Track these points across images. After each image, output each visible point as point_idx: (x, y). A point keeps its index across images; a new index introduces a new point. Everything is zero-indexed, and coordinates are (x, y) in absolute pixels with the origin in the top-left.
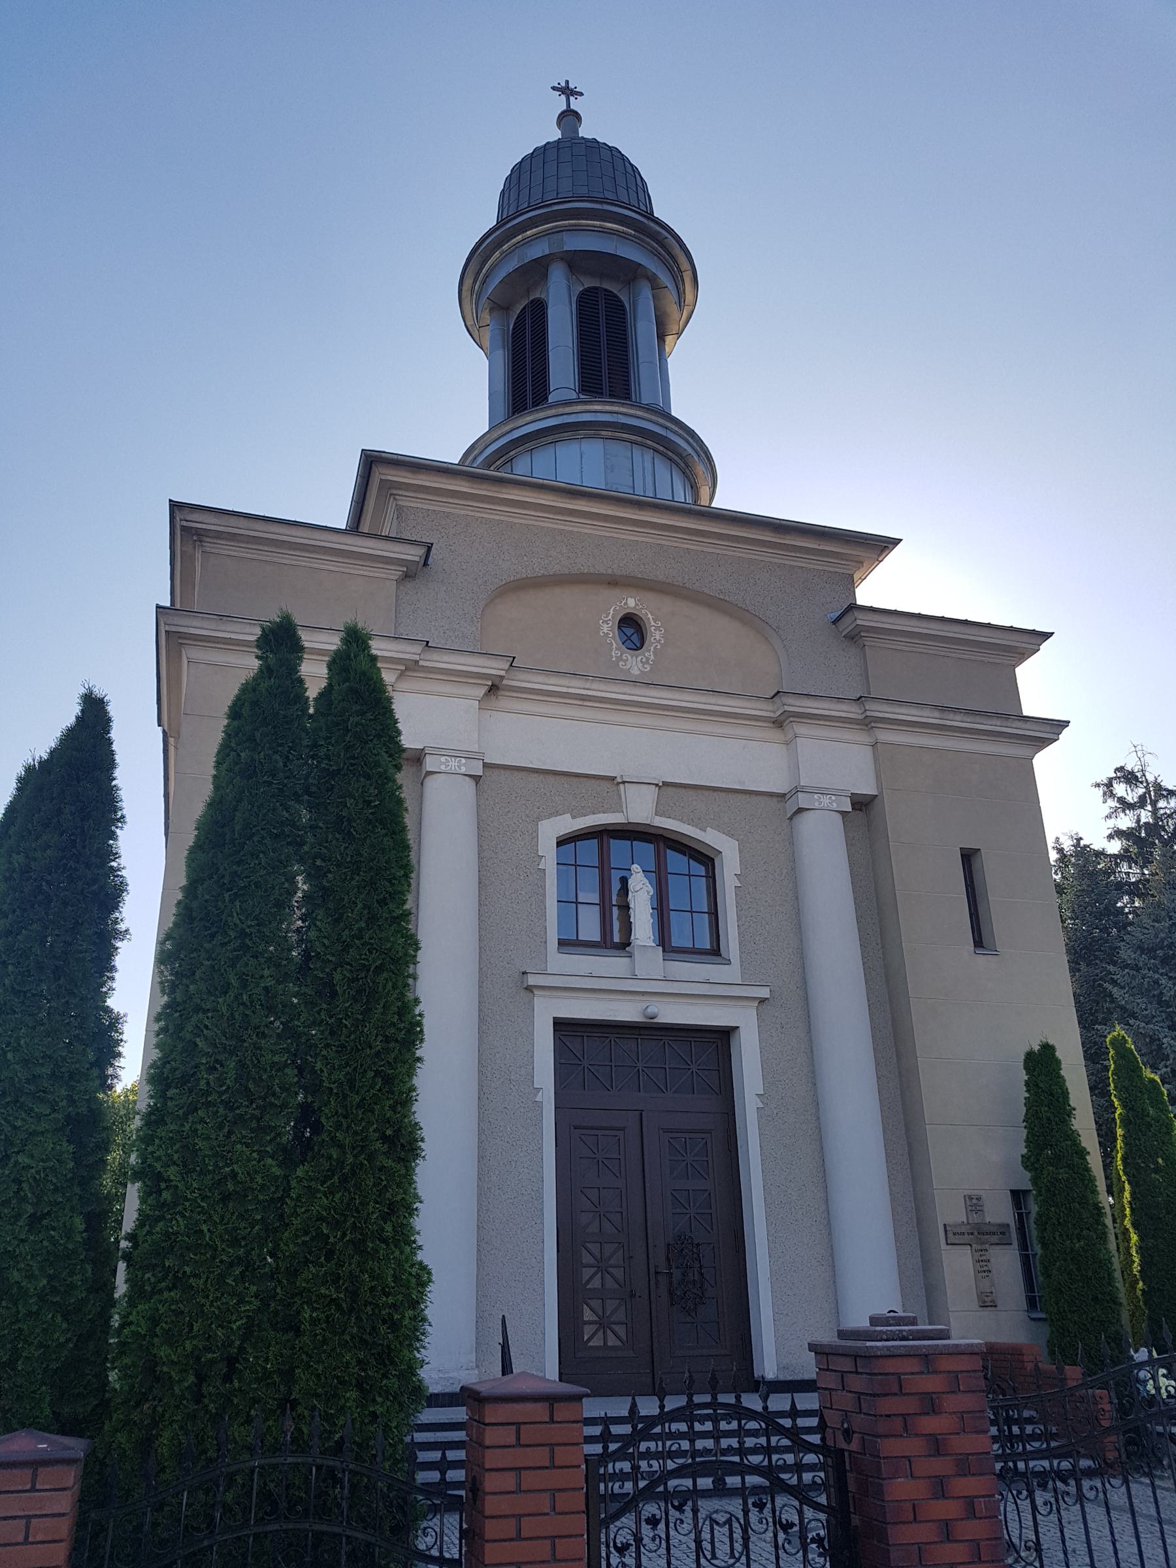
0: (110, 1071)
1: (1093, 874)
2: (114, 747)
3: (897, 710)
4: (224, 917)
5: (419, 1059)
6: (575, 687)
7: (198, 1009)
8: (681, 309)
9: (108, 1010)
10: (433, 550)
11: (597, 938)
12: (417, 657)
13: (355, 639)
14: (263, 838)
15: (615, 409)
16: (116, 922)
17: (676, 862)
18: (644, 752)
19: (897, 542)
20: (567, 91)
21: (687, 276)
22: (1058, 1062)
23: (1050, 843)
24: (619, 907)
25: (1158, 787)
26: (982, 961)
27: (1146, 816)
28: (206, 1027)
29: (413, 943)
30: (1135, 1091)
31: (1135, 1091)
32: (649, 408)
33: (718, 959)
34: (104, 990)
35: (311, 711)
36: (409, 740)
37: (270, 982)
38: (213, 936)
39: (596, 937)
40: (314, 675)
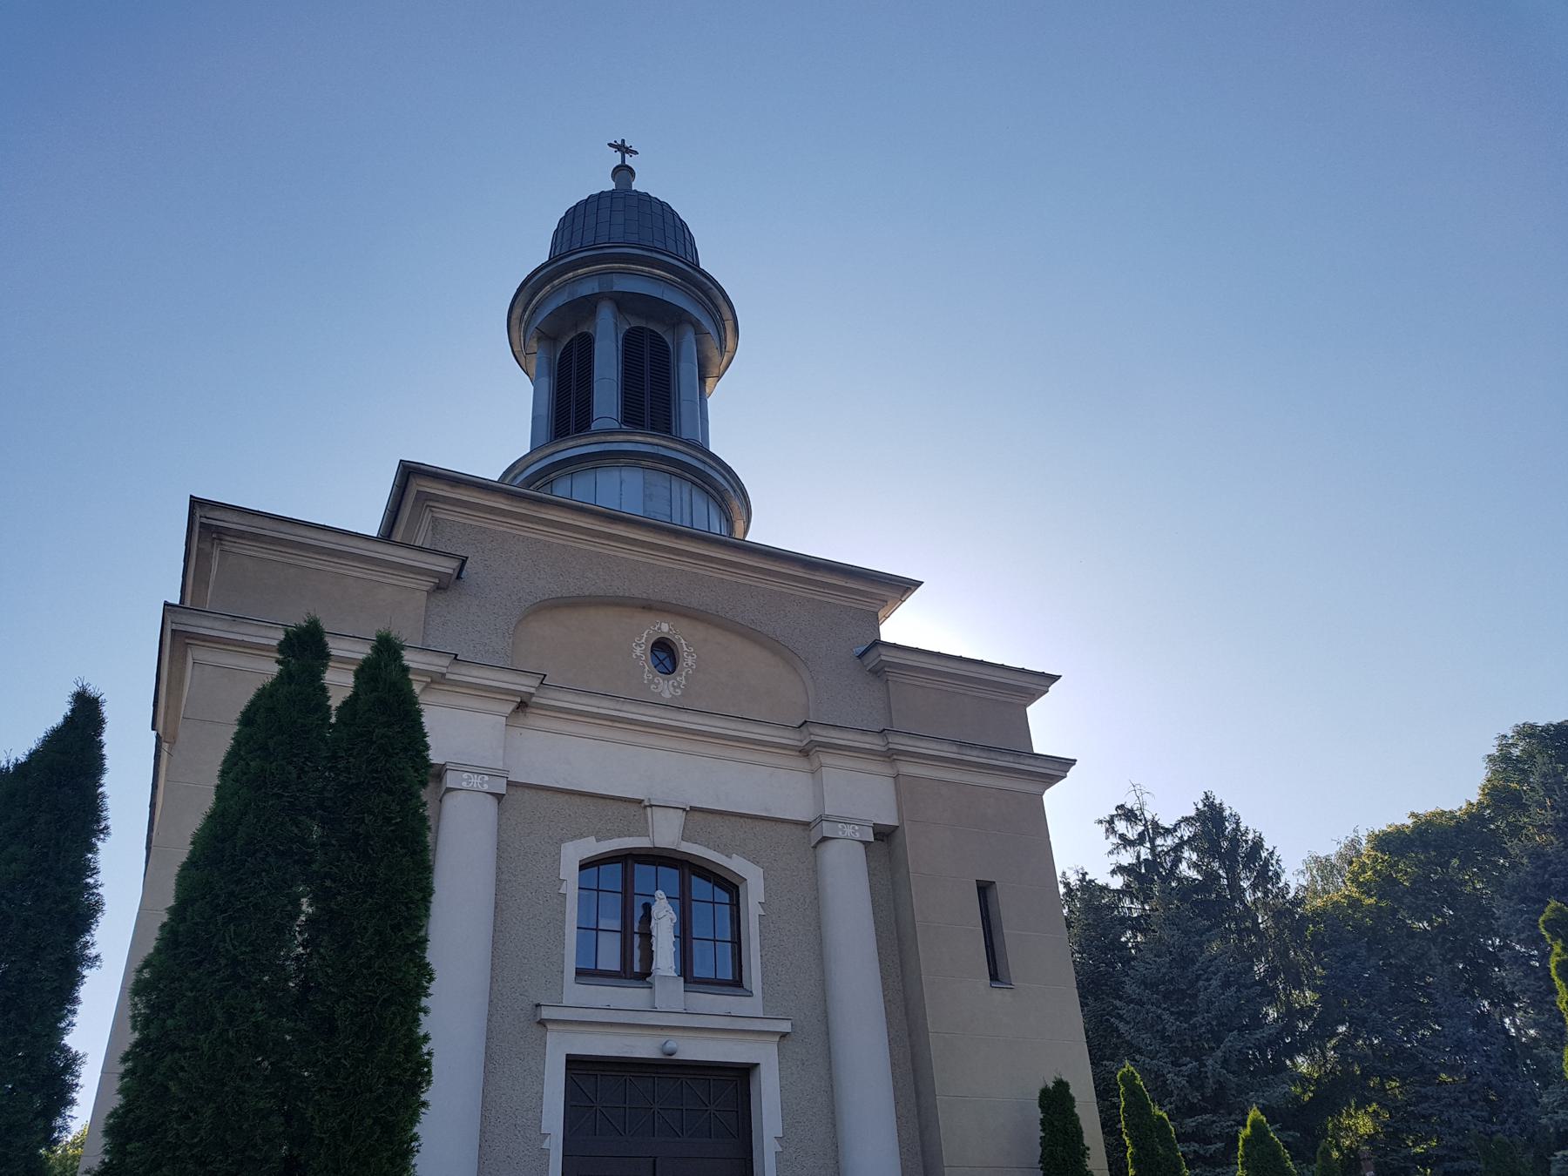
0: (59, 1122)
1: (1098, 909)
2: (105, 751)
4: (214, 943)
5: (424, 1104)
6: (606, 707)
7: (174, 1048)
8: (722, 355)
9: (65, 1050)
10: (468, 564)
11: (616, 967)
13: (387, 649)
14: (267, 855)
15: (656, 441)
16: (86, 946)
17: (700, 888)
18: (671, 778)
19: (918, 584)
20: (623, 149)
21: (729, 325)
22: (1072, 1099)
23: (1059, 874)
24: (641, 935)
25: (1155, 824)
26: (999, 995)
27: (1145, 853)
28: (182, 1069)
29: (425, 972)
30: (1145, 1130)
31: (1145, 1130)
32: (689, 443)
33: (739, 991)
34: (63, 1025)
35: (333, 720)
36: (435, 757)
37: (261, 1017)
38: (200, 963)
39: (616, 967)
40: (339, 683)
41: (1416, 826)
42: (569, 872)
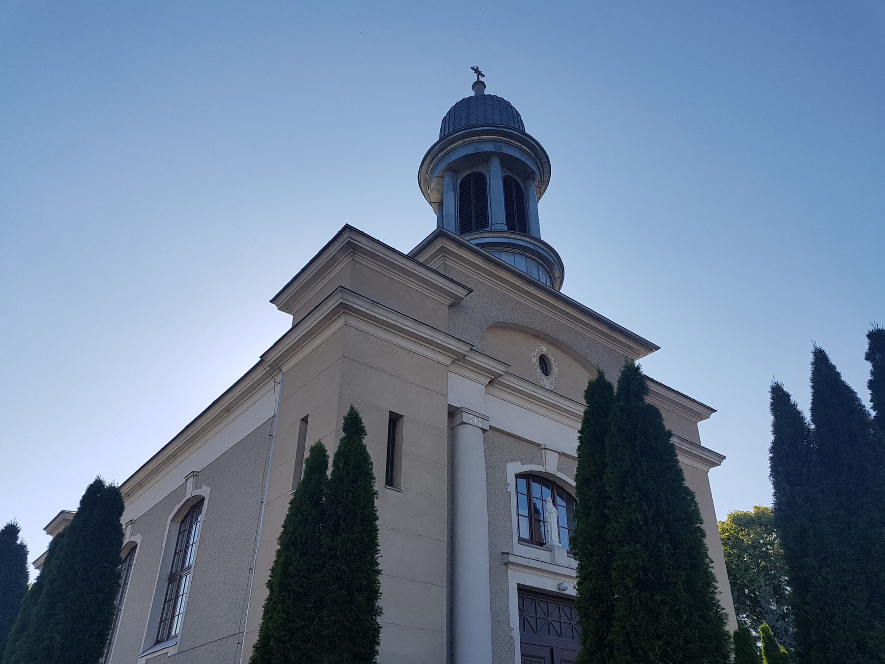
12: (466, 353)
19: (657, 348)
41: (756, 514)
42: (511, 479)
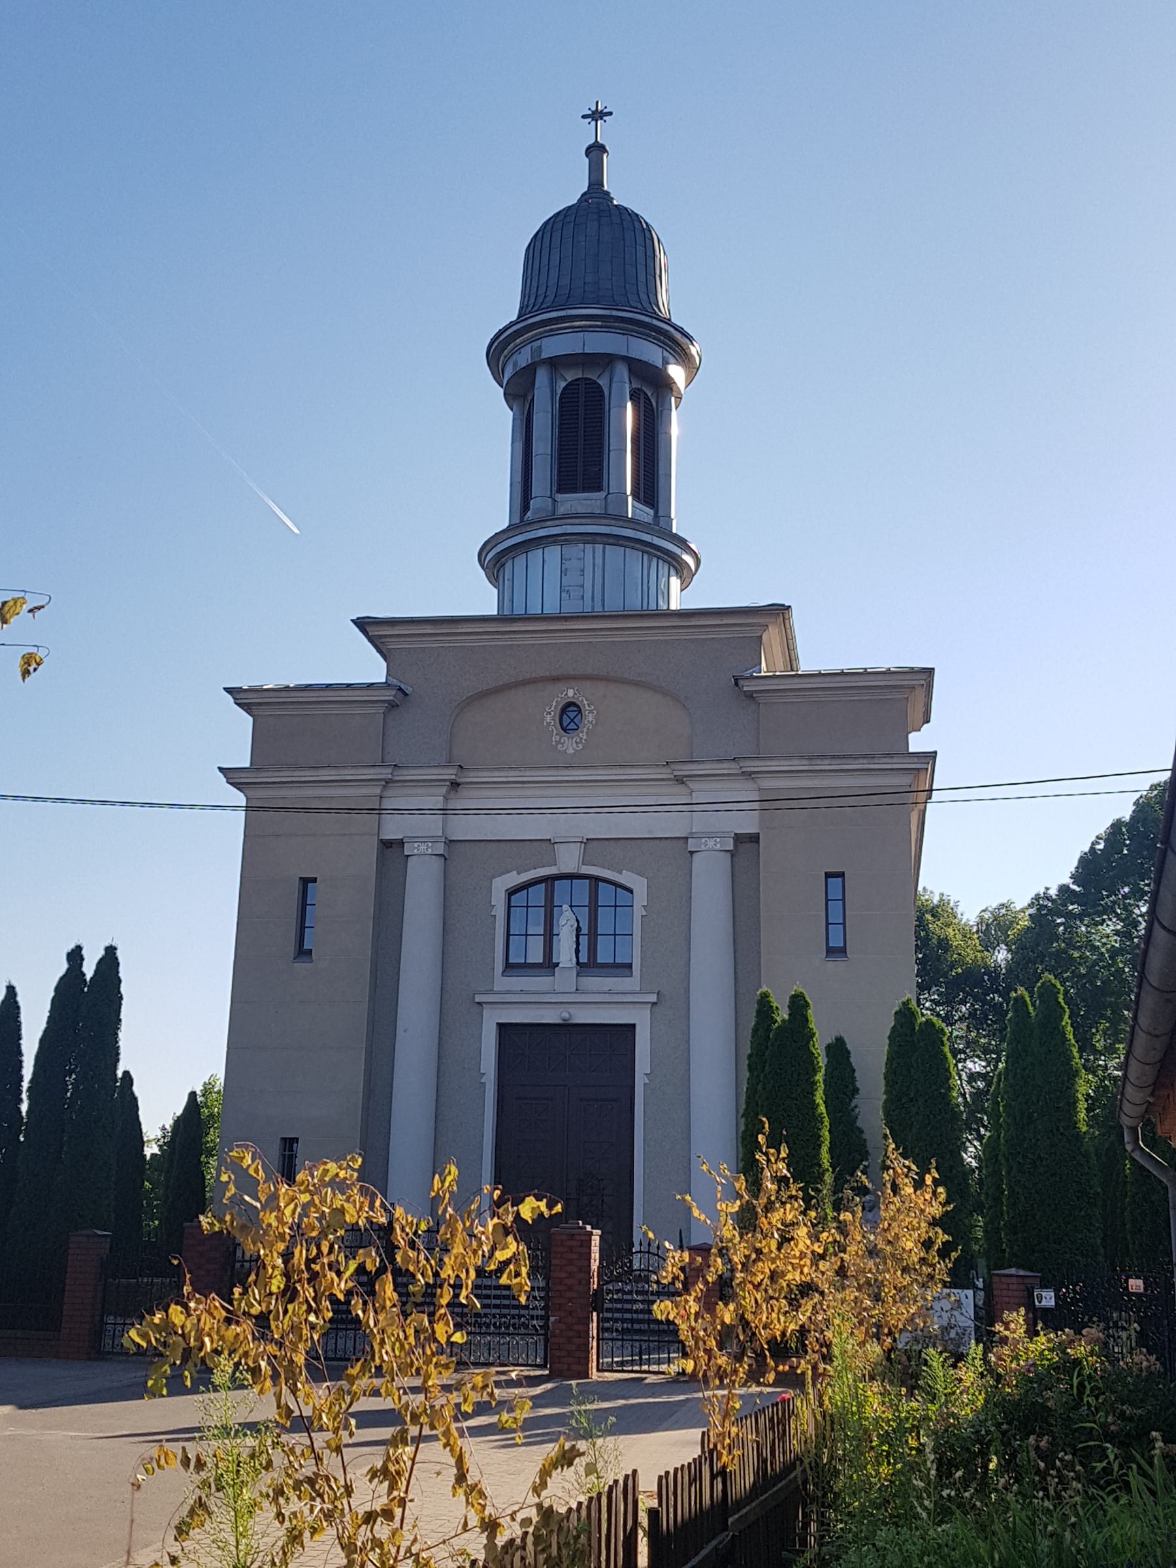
3: (768, 763)
6: (513, 776)
40: (89, 969)
